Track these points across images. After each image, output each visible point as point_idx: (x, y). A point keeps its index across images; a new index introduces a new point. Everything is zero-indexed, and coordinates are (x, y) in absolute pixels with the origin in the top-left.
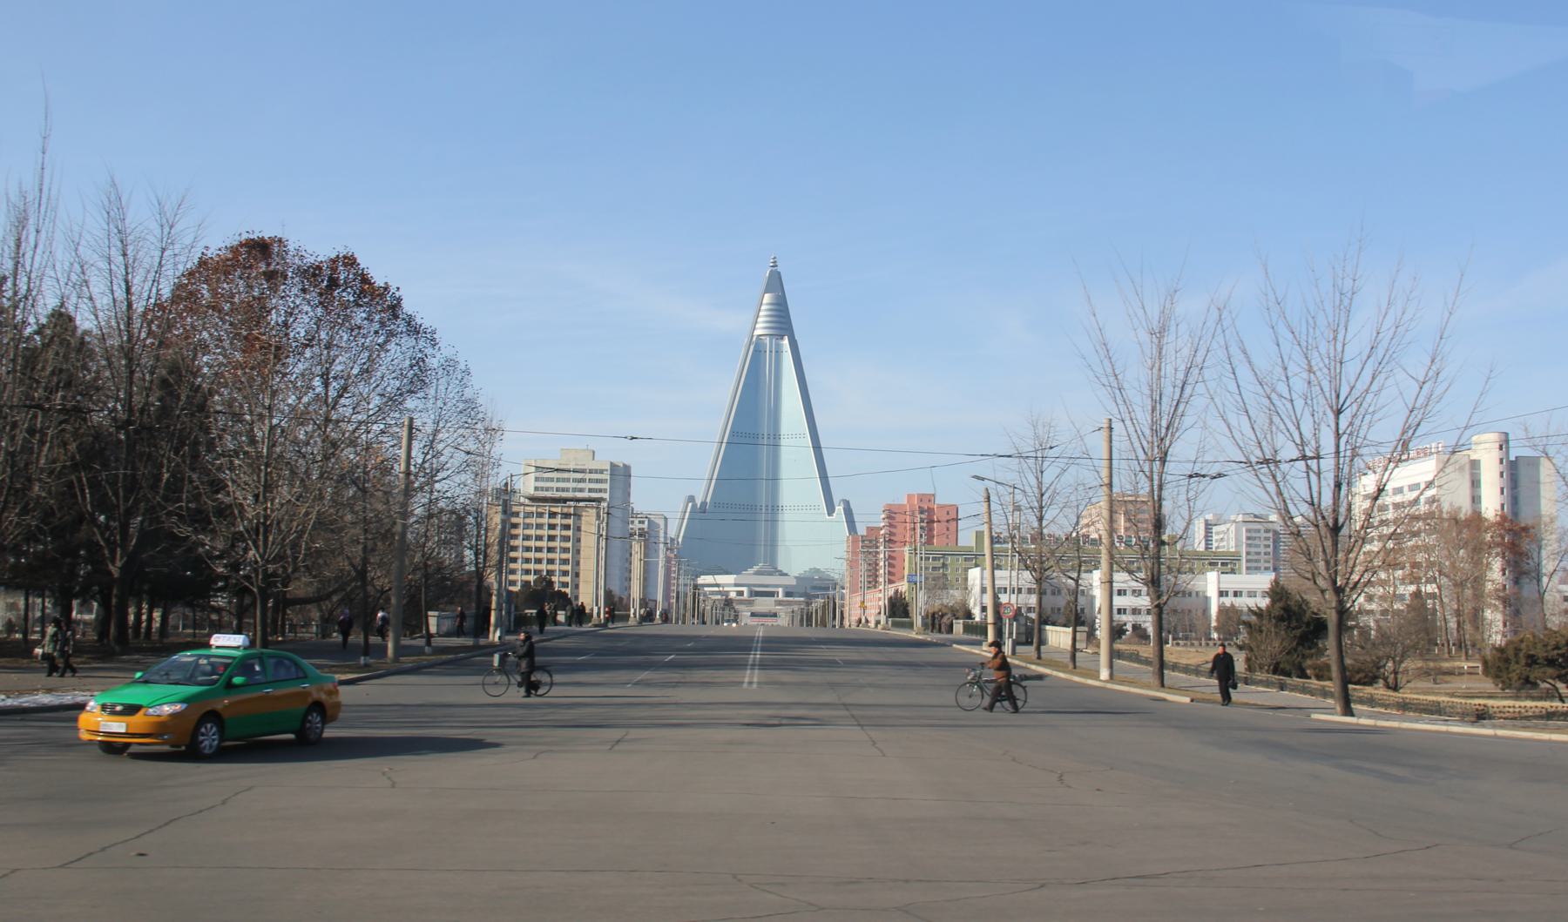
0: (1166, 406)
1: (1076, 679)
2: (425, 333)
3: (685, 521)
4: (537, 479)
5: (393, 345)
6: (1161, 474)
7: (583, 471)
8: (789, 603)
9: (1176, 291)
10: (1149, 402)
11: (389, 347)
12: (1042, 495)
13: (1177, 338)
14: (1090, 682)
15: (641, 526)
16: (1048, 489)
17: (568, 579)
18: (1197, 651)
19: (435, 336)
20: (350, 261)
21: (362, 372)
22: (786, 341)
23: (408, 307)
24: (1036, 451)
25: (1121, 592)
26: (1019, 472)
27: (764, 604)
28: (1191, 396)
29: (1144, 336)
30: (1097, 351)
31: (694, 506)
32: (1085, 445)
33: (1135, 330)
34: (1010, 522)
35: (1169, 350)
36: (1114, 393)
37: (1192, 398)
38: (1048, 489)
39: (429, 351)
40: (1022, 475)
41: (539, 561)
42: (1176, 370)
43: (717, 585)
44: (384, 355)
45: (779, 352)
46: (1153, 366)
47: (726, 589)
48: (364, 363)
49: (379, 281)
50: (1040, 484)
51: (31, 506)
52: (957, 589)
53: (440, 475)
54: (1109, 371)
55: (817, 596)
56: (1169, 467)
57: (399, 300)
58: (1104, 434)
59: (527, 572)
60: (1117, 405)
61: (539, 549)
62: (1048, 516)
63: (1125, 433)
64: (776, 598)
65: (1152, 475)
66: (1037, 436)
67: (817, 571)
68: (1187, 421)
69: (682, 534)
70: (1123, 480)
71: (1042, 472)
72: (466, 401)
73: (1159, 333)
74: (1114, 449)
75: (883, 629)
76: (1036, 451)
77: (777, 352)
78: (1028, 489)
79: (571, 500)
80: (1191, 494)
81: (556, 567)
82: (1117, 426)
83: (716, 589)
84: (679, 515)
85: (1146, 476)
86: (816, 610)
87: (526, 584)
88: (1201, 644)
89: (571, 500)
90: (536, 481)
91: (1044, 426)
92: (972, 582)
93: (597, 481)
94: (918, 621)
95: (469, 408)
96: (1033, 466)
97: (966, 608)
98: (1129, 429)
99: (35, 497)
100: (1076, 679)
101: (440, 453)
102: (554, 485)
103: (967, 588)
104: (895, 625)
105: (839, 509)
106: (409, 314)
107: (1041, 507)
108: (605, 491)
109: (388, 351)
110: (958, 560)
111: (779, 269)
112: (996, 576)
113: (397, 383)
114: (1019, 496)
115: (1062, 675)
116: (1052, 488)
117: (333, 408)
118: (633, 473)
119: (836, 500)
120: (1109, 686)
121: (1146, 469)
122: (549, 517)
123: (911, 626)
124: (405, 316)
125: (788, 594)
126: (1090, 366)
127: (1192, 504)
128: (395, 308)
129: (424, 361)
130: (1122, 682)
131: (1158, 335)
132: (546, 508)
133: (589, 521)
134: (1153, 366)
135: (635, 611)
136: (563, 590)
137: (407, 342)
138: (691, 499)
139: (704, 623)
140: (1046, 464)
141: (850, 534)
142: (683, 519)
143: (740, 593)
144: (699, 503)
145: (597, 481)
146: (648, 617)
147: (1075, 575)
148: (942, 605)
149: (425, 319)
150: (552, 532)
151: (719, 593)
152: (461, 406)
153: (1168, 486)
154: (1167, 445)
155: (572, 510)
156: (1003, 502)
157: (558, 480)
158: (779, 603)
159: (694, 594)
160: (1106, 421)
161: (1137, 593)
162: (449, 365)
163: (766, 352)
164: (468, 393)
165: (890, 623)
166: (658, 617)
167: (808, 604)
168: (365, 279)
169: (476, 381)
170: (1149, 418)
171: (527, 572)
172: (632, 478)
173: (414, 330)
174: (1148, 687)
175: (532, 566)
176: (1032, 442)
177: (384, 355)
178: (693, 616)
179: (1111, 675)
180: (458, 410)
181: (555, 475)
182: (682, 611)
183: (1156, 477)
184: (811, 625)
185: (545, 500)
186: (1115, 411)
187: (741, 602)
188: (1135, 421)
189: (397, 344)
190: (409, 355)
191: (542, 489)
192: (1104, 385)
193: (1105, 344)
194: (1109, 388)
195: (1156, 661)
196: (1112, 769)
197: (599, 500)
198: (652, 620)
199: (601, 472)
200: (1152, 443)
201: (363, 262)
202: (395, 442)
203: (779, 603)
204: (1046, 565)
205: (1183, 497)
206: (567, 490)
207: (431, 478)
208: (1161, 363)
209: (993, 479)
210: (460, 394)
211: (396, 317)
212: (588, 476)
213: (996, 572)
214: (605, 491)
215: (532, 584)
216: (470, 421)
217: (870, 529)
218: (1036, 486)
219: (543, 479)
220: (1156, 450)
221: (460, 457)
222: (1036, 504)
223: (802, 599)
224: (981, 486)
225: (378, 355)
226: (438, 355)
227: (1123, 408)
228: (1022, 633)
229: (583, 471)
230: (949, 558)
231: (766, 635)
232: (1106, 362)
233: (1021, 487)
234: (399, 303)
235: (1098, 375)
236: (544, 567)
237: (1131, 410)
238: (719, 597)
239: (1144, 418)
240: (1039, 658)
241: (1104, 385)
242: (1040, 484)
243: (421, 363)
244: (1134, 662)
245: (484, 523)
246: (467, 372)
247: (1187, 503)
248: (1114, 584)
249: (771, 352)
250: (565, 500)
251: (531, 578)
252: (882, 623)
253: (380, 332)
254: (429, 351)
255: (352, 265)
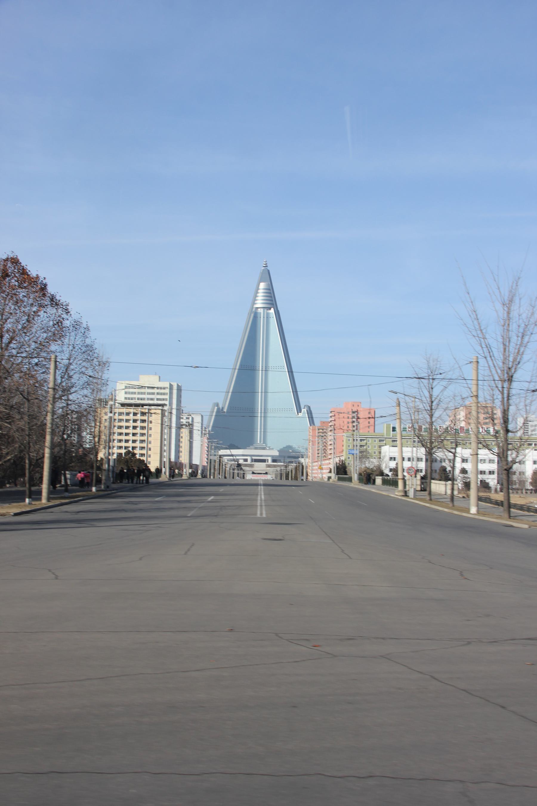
0: (512, 348)
1: (456, 512)
2: (62, 305)
3: (213, 417)
4: (126, 393)
5: (42, 312)
6: (509, 389)
7: (153, 388)
8: (275, 466)
9: (519, 278)
10: (501, 346)
11: (39, 314)
12: (432, 402)
13: (520, 307)
14: (464, 514)
15: (187, 420)
16: (436, 398)
17: (144, 452)
18: (520, 497)
19: (68, 307)
20: (15, 261)
21: (24, 328)
22: (272, 311)
23: (51, 290)
24: (429, 376)
25: (484, 461)
26: (419, 389)
27: (259, 467)
28: (528, 342)
29: (499, 306)
30: (470, 316)
31: (218, 409)
32: (462, 372)
33: (493, 302)
34: (413, 418)
35: (514, 314)
36: (480, 340)
37: (529, 344)
38: (436, 398)
39: (64, 316)
40: (420, 390)
41: (127, 441)
42: (519, 326)
43: (232, 455)
44: (37, 318)
45: (268, 317)
46: (505, 324)
47: (238, 457)
48: (25, 323)
49: (33, 274)
50: (431, 396)
51: (31, 436)
52: (375, 458)
53: (73, 390)
54: (477, 327)
55: (292, 462)
56: (514, 385)
57: (45, 285)
58: (474, 365)
59: (120, 447)
60: (482, 348)
61: (127, 434)
62: (436, 414)
63: (487, 365)
64: (267, 463)
65: (503, 390)
66: (429, 368)
67: (289, 447)
68: (526, 357)
69: (211, 424)
70: (486, 394)
71: (432, 388)
72: (87, 346)
73: (508, 304)
74: (479, 374)
75: (333, 482)
76: (429, 376)
77: (267, 317)
78: (424, 399)
79: (146, 405)
80: (528, 401)
81: (138, 444)
82: (482, 361)
83: (231, 458)
84: (209, 414)
85: (499, 390)
86: (292, 470)
87: (120, 455)
88: (522, 493)
89: (146, 405)
90: (125, 394)
91: (433, 361)
92: (384, 454)
93: (161, 394)
94: (355, 477)
95: (89, 349)
96: (426, 385)
97: (380, 469)
98: (489, 362)
99: (45, 423)
100: (456, 512)
101: (71, 377)
102: (136, 396)
103: (380, 458)
104: (340, 479)
105: (304, 410)
106: (52, 294)
107: (431, 409)
108: (166, 400)
109: (39, 316)
110: (375, 441)
111: (268, 268)
112: (403, 451)
113: (45, 335)
114: (418, 403)
115: (446, 510)
116: (438, 398)
117: (6, 349)
118: (182, 388)
119: (302, 406)
120: (477, 517)
121: (500, 386)
122: (119, 415)
123: (350, 480)
124: (49, 295)
125: (274, 461)
126: (465, 324)
127: (528, 408)
128: (44, 288)
129: (61, 323)
130: (484, 515)
131: (507, 305)
132: (132, 410)
133: (156, 418)
134: (505, 324)
135: (187, 471)
136: (142, 458)
137: (51, 311)
138: (217, 405)
139: (225, 478)
140: (434, 384)
141: (310, 425)
142: (212, 415)
143: (246, 460)
144: (221, 406)
145: (161, 394)
146: (194, 474)
147: (453, 450)
148: (366, 467)
149: (62, 297)
150: (135, 424)
151: (234, 460)
152: (84, 349)
153: (513, 397)
154: (513, 372)
155: (147, 411)
156: (409, 407)
157: (139, 393)
158: (269, 466)
159: (220, 461)
160: (475, 358)
161: (491, 461)
162: (77, 325)
163: (261, 317)
164: (88, 341)
165: (337, 478)
166: (199, 474)
167: (286, 467)
168: (24, 272)
169: (93, 334)
170: (502, 356)
171: (120, 447)
172: (182, 391)
173: (54, 302)
174: (500, 517)
175: (123, 444)
176: (426, 371)
177: (37, 318)
178: (219, 474)
179: (478, 511)
180: (82, 351)
181: (137, 390)
182: (212, 471)
183: (506, 392)
184: (288, 479)
185: (130, 405)
186: (481, 352)
187: (246, 465)
188: (493, 358)
189: (45, 312)
190: (52, 318)
191: (129, 399)
192: (474, 336)
193: (475, 311)
194: (477, 338)
195: (506, 504)
196: (491, 568)
197: (163, 405)
198: (196, 476)
199: (164, 388)
200: (504, 371)
201: (24, 261)
202: (44, 370)
203: (269, 466)
204: (433, 445)
205: (522, 404)
206: (144, 399)
207: (67, 391)
208: (509, 322)
209: (403, 393)
210: (83, 342)
211: (44, 295)
212: (156, 391)
213: (404, 448)
214: (166, 400)
215: (123, 455)
216: (89, 358)
217: (323, 423)
218: (429, 397)
219: (129, 393)
220: (506, 375)
221: (85, 379)
222: (429, 408)
223: (282, 464)
224: (395, 396)
225: (33, 319)
226: (70, 319)
227: (485, 349)
228: (418, 485)
229: (153, 388)
230: (370, 439)
231: (264, 483)
232: (476, 322)
233: (419, 397)
234: (45, 287)
235: (471, 330)
236: (130, 444)
237: (490, 351)
238: (233, 462)
239: (498, 355)
240: (431, 500)
241: (474, 336)
242: (431, 396)
243: (60, 324)
244: (488, 503)
245: (98, 419)
246: (87, 329)
247: (524, 407)
248: (479, 456)
249: (264, 317)
250: (143, 405)
251: (123, 451)
252: (332, 478)
253: (34, 304)
254: (64, 316)
255: (16, 263)
